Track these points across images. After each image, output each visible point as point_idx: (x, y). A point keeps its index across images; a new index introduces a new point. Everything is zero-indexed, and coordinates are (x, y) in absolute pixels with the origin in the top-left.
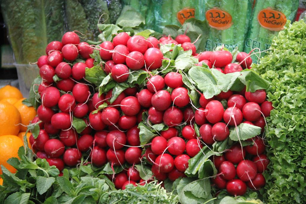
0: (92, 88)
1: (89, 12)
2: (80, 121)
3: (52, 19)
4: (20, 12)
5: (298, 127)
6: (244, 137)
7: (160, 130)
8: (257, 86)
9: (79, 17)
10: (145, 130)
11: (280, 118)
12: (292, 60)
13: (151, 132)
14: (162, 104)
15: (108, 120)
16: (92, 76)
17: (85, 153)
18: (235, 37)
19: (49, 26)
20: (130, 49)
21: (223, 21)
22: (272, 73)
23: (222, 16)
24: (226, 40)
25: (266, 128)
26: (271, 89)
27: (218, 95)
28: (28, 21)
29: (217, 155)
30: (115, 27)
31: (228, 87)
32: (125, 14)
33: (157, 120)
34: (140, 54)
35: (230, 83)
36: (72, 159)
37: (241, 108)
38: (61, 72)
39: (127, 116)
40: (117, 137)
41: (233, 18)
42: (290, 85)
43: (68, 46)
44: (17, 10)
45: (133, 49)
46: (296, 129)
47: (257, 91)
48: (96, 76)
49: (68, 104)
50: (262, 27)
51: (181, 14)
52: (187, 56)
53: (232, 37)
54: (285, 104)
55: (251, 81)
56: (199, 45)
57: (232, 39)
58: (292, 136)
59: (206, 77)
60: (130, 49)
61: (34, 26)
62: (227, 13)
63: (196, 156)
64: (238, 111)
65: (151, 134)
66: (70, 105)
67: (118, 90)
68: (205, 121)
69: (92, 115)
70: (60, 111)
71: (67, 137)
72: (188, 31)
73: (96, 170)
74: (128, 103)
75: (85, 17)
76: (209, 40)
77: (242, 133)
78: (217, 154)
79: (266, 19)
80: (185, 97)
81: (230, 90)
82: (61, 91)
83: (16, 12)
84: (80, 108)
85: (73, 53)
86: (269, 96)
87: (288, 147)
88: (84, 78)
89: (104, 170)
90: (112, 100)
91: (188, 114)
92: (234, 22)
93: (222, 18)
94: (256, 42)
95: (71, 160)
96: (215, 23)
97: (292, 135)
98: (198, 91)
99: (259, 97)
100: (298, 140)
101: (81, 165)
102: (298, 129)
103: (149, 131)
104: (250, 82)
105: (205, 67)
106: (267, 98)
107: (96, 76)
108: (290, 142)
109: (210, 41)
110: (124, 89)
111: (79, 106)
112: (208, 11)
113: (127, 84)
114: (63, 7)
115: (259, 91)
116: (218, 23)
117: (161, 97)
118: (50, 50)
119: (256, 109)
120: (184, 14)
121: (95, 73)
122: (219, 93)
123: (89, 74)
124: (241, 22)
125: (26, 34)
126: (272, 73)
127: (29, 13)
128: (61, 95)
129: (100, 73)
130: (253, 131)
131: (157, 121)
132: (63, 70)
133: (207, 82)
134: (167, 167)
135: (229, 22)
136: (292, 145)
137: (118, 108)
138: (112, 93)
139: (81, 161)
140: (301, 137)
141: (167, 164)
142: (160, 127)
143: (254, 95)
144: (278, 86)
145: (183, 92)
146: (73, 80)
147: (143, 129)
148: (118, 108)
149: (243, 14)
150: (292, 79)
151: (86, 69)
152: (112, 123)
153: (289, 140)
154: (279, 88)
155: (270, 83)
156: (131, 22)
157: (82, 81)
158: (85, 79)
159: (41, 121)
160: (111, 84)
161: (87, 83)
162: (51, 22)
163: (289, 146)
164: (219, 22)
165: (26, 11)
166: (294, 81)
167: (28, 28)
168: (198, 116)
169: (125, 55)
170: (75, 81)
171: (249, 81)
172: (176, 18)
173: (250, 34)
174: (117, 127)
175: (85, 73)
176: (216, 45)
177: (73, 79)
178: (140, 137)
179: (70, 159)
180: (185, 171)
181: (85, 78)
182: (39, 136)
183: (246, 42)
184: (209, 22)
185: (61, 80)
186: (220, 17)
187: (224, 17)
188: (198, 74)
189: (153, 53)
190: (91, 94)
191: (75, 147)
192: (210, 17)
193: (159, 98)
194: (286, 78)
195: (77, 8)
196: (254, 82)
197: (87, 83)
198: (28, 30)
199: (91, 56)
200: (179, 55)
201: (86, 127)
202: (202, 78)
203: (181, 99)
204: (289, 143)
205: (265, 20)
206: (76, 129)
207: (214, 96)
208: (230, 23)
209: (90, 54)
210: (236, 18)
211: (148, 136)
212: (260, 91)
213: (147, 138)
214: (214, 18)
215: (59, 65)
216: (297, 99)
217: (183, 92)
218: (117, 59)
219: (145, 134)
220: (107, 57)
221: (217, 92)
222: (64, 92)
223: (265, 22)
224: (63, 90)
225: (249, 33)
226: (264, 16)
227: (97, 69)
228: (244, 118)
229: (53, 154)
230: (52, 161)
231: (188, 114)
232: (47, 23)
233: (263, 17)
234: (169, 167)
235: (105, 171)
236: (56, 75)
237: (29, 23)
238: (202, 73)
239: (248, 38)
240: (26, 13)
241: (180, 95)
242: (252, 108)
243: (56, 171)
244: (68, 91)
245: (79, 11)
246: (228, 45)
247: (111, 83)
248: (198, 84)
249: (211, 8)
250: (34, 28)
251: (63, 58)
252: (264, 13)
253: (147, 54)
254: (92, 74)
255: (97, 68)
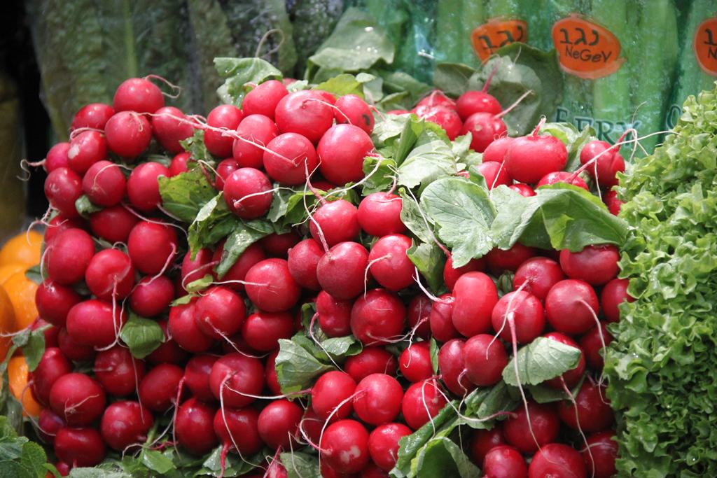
0: (178, 233)
1: (239, 27)
2: (146, 326)
3: (150, 45)
4: (63, 27)
5: (679, 352)
6: (536, 376)
7: (340, 354)
8: (588, 234)
9: (215, 39)
10: (294, 353)
11: (639, 324)
12: (705, 164)
13: (314, 359)
14: (341, 279)
15: (207, 323)
16: (181, 199)
17: (157, 414)
18: (633, 101)
19: (143, 65)
20: (281, 125)
21: (593, 53)
22: (646, 199)
23: (590, 38)
24: (606, 107)
25: (603, 352)
26: (633, 244)
27: (483, 255)
28: (85, 52)
29: (474, 426)
30: (265, 65)
31: (512, 235)
32: (345, 33)
33: (337, 327)
34: (301, 142)
35: (519, 223)
36: (122, 430)
37: (540, 294)
38: (95, 188)
39: (264, 314)
40: (237, 370)
41: (622, 44)
42: (687, 233)
43: (121, 118)
44: (57, 20)
45: (287, 127)
46: (674, 357)
47: (588, 247)
48: (193, 202)
49: (110, 276)
50: (703, 71)
51: (480, 38)
52: (436, 150)
53: (621, 99)
54: (655, 287)
55: (572, 219)
56: (528, 122)
57: (621, 106)
58: (665, 378)
59: (471, 208)
60: (281, 125)
61: (103, 65)
62: (604, 30)
63: (422, 428)
64: (531, 302)
65: (310, 364)
66: (117, 279)
67: (242, 240)
68: (453, 331)
69: (175, 307)
70: (94, 297)
71: (110, 369)
72: (495, 80)
73: (189, 465)
74: (263, 277)
75: (229, 40)
76: (564, 108)
77: (531, 365)
78: (474, 423)
79: (569, 46)
80: (401, 262)
81: (518, 244)
82: (101, 242)
83: (55, 25)
84: (149, 289)
85: (132, 136)
86: (623, 264)
87: (656, 409)
88: (159, 206)
89: (206, 464)
90: (223, 268)
91: (416, 310)
92: (626, 58)
93: (590, 44)
94: (564, 113)
95: (118, 434)
96: (573, 59)
97: (665, 374)
98: (441, 246)
99: (594, 267)
100: (682, 389)
101: (145, 449)
102: (680, 356)
103: (306, 354)
104: (569, 222)
105: (477, 180)
106: (618, 270)
107: (193, 202)
108: (660, 393)
109: (566, 112)
110: (257, 238)
111: (145, 284)
112: (556, 24)
113: (267, 225)
114: (179, 13)
115: (597, 249)
116: (582, 59)
117: (338, 260)
118: (76, 128)
119: (579, 299)
120: (489, 35)
121: (188, 191)
122: (485, 252)
123: (172, 196)
124: (650, 58)
125: (82, 89)
126: (646, 199)
127: (89, 30)
128: (97, 249)
129: (200, 192)
130: (557, 359)
131: (337, 330)
132: (99, 180)
133: (471, 222)
134: (345, 456)
135: (612, 55)
136: (665, 402)
137: (239, 291)
138: (224, 249)
139: (147, 437)
140: (688, 379)
141: (347, 448)
142: (341, 345)
143: (582, 259)
144: (653, 237)
145: (398, 249)
146: (131, 211)
147: (287, 348)
148: (239, 291)
149: (655, 34)
150: (692, 218)
151: (160, 179)
152: (218, 331)
153: (657, 390)
154: (657, 243)
155: (631, 228)
156: (349, 56)
157: (156, 214)
158: (161, 209)
159: (48, 326)
160: (224, 224)
161: (168, 219)
162: (148, 55)
163: (657, 404)
164: (583, 56)
165: (78, 22)
166: (696, 224)
167: (85, 71)
168: (437, 316)
169: (256, 142)
170: (136, 214)
171: (566, 218)
172: (470, 48)
173: (677, 93)
174: (232, 343)
175: (160, 190)
176: (577, 122)
177: (131, 207)
178: (276, 369)
179: (115, 430)
180: (389, 472)
181: (162, 206)
182: (40, 363)
183: (668, 114)
184: (560, 57)
185: (97, 210)
186: (585, 43)
187: (595, 42)
188: (447, 199)
189: (345, 139)
190: (176, 251)
191: (132, 397)
192: (562, 42)
193: (332, 262)
194: (679, 216)
195: (209, 15)
196: (583, 221)
197: (168, 219)
198: (85, 76)
199: (183, 145)
200: (418, 146)
201: (162, 343)
202: (457, 209)
203: (391, 268)
204: (659, 396)
205: (710, 50)
206: (129, 345)
207: (472, 260)
208: (616, 60)
209: (180, 141)
210: (633, 47)
211: (302, 369)
212: (600, 248)
213: (299, 375)
214: (571, 43)
215: (92, 168)
216: (686, 273)
217: (396, 248)
218: (241, 154)
219: (292, 361)
220: (222, 151)
221: (483, 248)
222: (107, 244)
223: (711, 56)
224: (106, 239)
225: (674, 92)
226: (707, 40)
227: (192, 180)
228: (547, 324)
229: (68, 413)
230: (70, 434)
231: (416, 310)
232: (139, 58)
233: (706, 43)
234: (352, 456)
235: (208, 469)
236: (84, 197)
237: (87, 58)
238: (462, 197)
239: (672, 103)
240: (79, 29)
241: (389, 256)
242: (572, 294)
243: (13, 448)
244: (118, 241)
245: (215, 23)
246: (610, 124)
247: (225, 221)
248: (441, 227)
249: (563, 17)
250: (102, 72)
251: (107, 150)
252: (707, 31)
253: (324, 142)
254: (182, 196)
255: (191, 178)
